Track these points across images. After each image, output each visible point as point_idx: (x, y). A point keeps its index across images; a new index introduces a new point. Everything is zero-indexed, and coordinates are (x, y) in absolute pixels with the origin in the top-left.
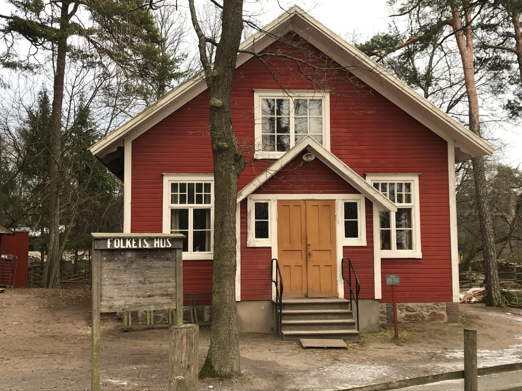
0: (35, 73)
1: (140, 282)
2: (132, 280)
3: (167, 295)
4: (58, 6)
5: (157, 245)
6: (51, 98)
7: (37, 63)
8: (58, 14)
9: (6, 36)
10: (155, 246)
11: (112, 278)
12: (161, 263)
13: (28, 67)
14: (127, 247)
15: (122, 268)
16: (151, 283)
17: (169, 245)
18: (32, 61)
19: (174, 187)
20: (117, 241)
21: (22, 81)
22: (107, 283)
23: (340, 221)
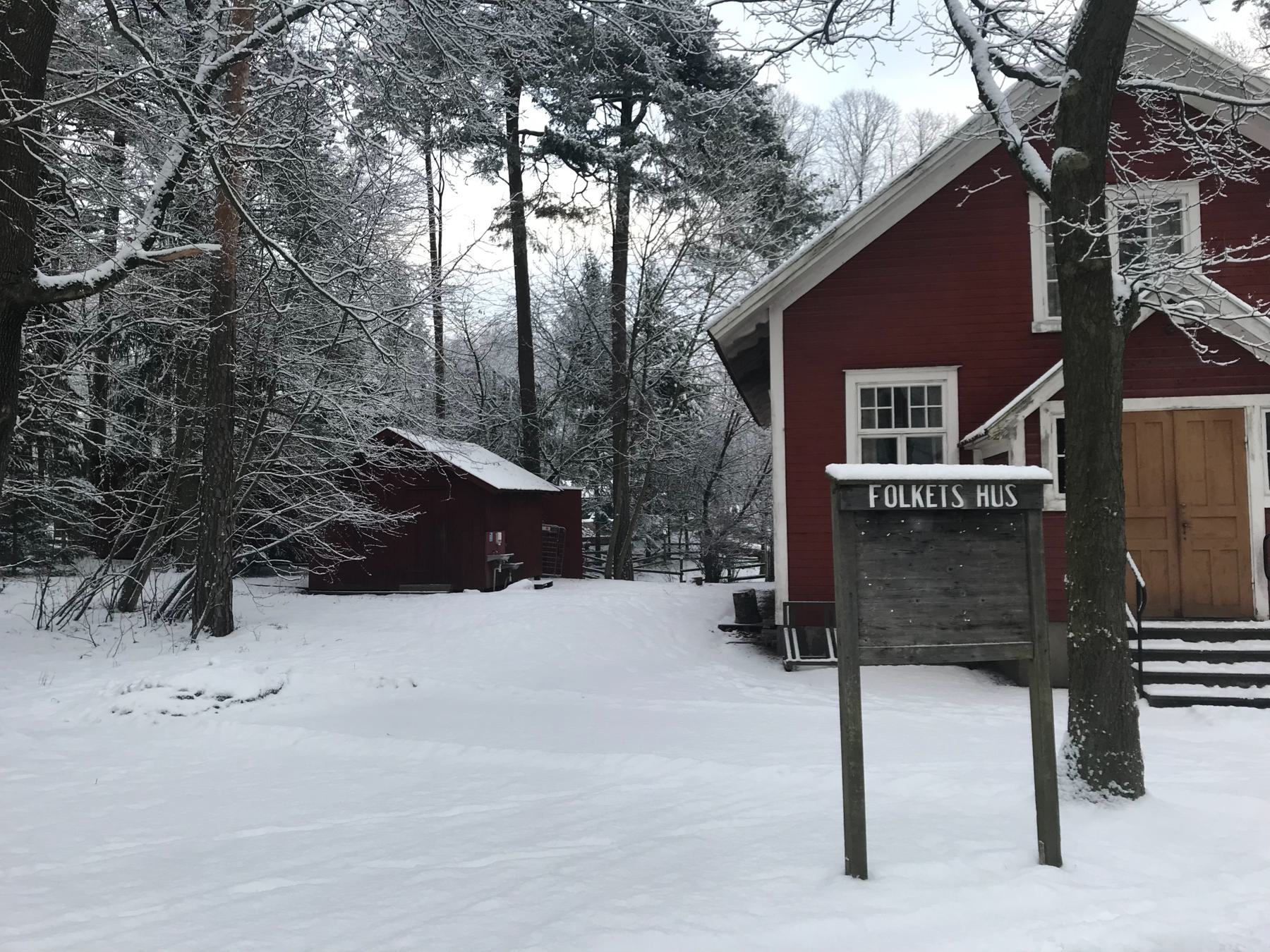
0: (586, 224)
1: (946, 592)
2: (928, 587)
3: (1010, 624)
4: (616, 107)
5: (983, 502)
6: (606, 271)
7: (588, 206)
8: (616, 121)
9: (538, 164)
10: (979, 505)
11: (880, 581)
12: (993, 546)
13: (575, 214)
14: (914, 505)
15: (901, 556)
16: (971, 594)
17: (1011, 502)
18: (580, 203)
19: (866, 395)
20: (890, 489)
21: (568, 235)
22: (871, 593)
23: (1257, 455)
